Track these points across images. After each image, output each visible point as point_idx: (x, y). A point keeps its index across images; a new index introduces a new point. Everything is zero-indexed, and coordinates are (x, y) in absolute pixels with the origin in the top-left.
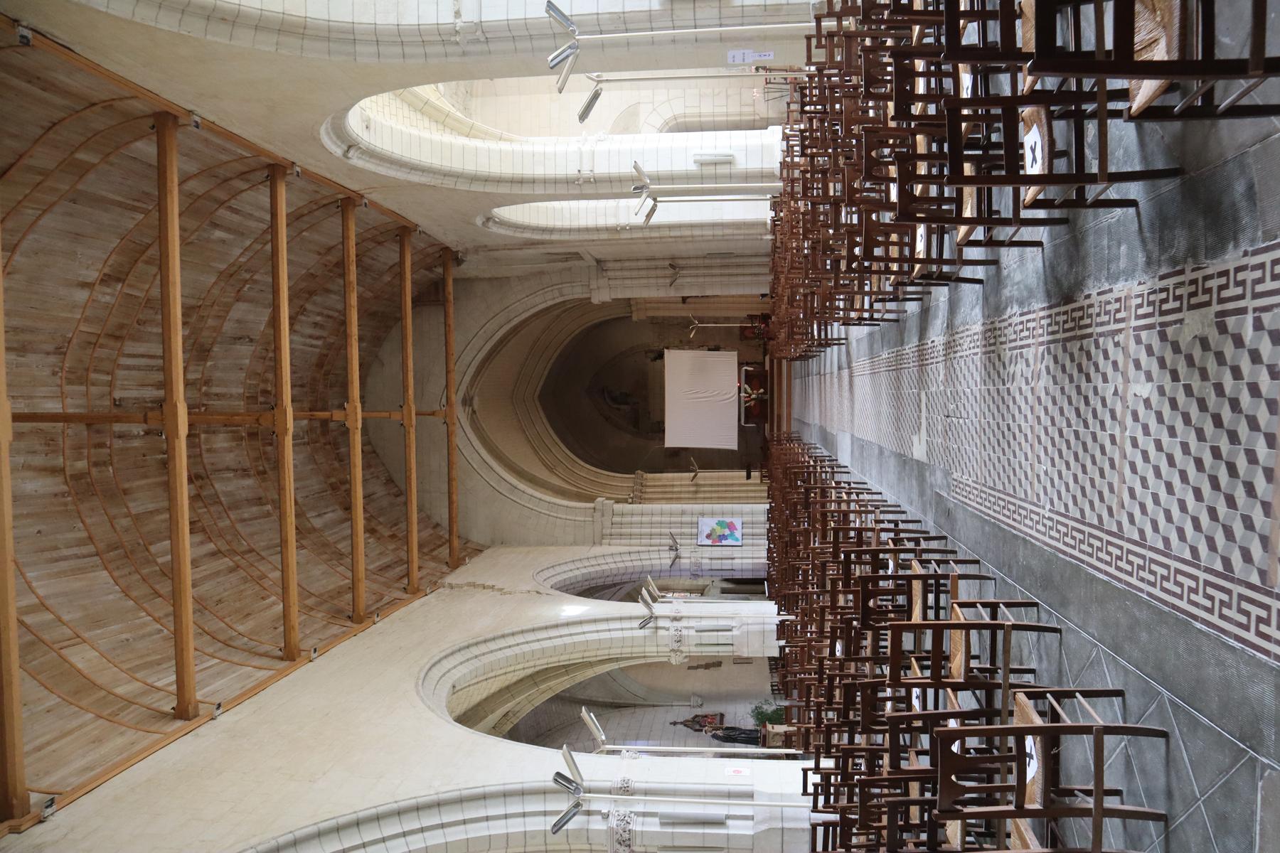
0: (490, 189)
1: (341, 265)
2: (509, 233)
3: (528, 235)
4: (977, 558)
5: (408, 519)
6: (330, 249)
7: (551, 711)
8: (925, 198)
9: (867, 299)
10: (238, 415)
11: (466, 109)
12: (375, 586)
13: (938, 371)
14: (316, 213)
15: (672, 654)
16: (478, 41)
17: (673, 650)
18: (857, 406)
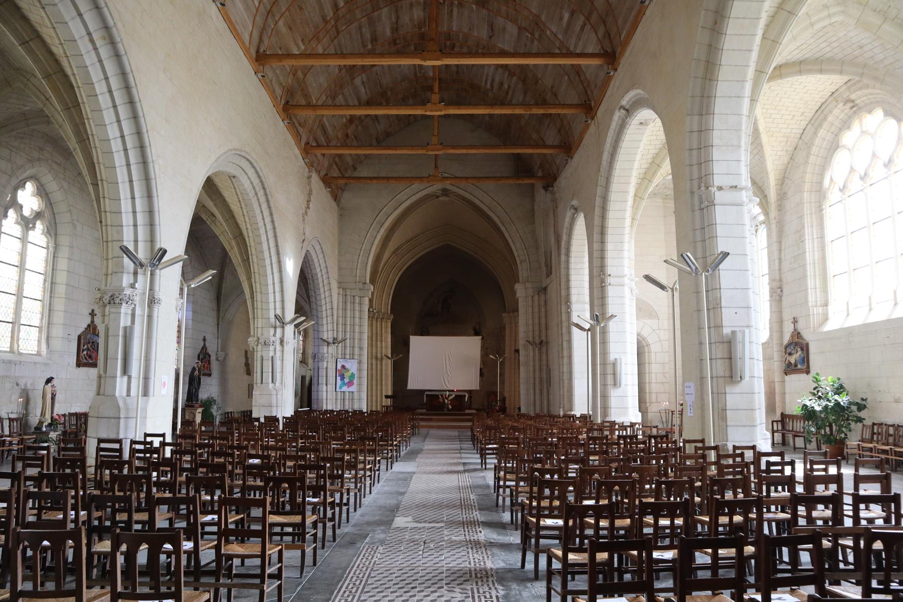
0: (597, 211)
1: (544, 103)
2: (566, 225)
3: (564, 238)
4: (318, 564)
5: (359, 147)
6: (555, 95)
7: (216, 250)
8: (583, 526)
9: (514, 483)
10: (437, 25)
11: (654, 194)
12: (311, 121)
13: (459, 535)
14: (581, 86)
15: (256, 339)
16: (701, 202)
17: (258, 339)
18: (436, 476)
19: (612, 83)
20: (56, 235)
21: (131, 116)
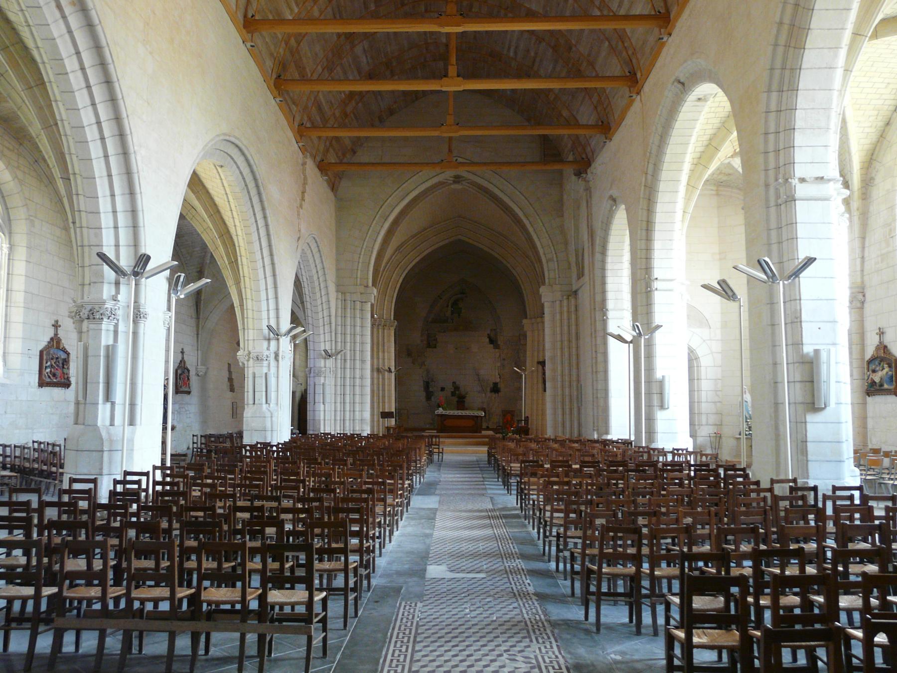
1: (578, 74)
6: (592, 64)
15: (246, 352)
16: (778, 196)
17: (250, 353)
19: (665, 50)
20: (10, 233)
21: (108, 98)
